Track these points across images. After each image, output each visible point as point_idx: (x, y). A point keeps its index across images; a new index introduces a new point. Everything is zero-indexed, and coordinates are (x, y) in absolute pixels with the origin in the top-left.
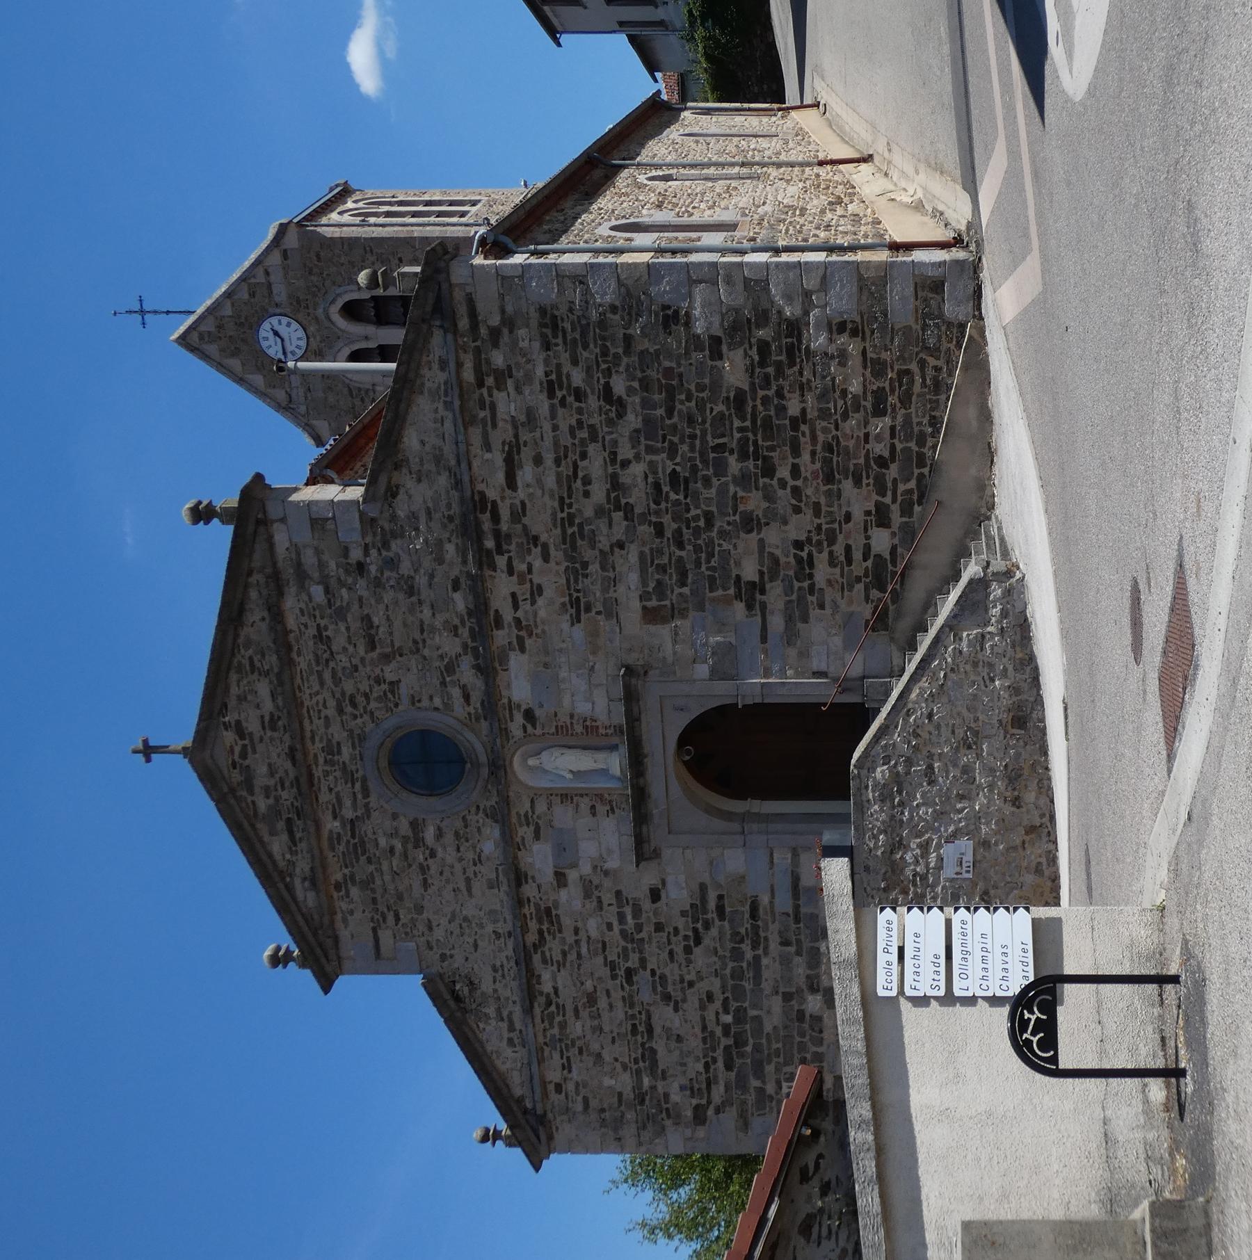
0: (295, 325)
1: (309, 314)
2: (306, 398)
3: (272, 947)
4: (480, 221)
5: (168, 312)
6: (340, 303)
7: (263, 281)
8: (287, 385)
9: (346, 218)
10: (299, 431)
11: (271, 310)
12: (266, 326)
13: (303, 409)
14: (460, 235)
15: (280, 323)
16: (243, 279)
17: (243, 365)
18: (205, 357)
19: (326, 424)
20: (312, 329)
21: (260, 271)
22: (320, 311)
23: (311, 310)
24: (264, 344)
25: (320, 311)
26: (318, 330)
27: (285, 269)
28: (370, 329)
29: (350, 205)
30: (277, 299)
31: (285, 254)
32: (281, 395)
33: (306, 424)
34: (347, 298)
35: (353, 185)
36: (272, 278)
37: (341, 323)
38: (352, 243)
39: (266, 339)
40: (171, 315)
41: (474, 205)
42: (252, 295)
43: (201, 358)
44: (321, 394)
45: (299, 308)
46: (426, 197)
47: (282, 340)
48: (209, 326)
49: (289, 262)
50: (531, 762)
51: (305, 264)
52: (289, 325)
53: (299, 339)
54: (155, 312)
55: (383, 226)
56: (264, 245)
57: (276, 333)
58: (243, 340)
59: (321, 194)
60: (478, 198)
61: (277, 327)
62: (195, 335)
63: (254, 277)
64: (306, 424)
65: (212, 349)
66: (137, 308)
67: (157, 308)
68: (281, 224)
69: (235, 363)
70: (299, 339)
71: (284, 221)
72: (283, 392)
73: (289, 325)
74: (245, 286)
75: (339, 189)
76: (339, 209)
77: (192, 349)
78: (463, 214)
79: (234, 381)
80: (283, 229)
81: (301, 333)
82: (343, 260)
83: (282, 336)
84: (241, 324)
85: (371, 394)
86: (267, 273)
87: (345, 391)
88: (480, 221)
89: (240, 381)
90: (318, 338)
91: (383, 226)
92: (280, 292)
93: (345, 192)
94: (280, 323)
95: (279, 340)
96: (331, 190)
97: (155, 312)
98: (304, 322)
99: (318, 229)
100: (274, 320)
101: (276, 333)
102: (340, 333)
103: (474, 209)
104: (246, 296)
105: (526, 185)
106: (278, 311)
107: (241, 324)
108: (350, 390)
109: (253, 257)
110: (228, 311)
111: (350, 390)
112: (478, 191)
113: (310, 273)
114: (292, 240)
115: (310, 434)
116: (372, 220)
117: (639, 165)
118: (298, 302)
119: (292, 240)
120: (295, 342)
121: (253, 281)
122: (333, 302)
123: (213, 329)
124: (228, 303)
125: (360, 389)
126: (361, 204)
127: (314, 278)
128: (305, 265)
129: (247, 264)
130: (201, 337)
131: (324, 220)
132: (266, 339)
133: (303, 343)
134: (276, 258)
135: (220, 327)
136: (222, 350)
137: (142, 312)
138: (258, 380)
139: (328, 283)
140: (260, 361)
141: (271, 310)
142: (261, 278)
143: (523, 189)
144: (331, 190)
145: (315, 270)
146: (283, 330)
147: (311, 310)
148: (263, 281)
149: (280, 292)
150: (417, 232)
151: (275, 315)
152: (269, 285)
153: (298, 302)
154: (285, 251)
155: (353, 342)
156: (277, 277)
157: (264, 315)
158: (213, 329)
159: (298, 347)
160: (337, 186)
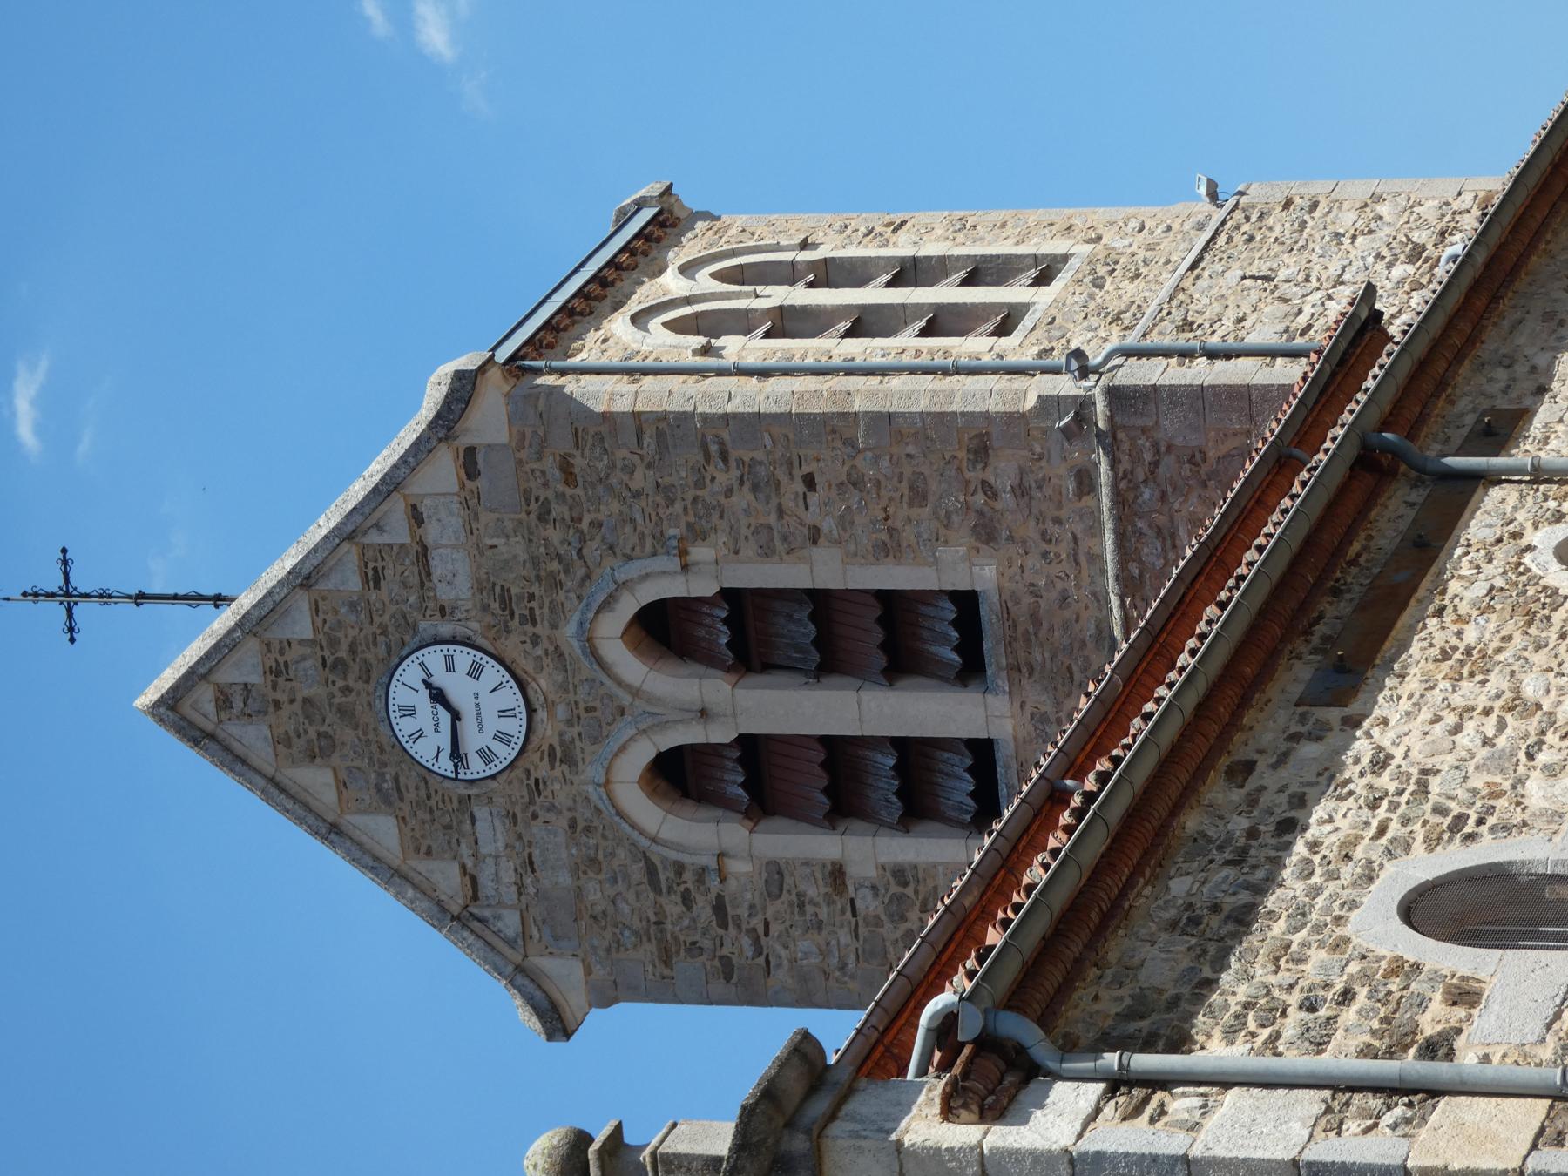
0: (493, 673)
1: (535, 640)
2: (521, 889)
3: (613, 1123)
4: (1059, 358)
5: (141, 598)
6: (628, 607)
7: (406, 539)
8: (465, 850)
9: (660, 342)
10: (498, 987)
11: (426, 626)
12: (410, 673)
13: (510, 923)
14: (994, 406)
15: (450, 666)
16: (347, 533)
17: (342, 785)
18: (234, 761)
19: (577, 968)
20: (543, 683)
21: (396, 510)
22: (569, 630)
23: (542, 629)
24: (404, 727)
25: (569, 630)
26: (563, 687)
27: (471, 504)
28: (715, 688)
29: (671, 283)
30: (445, 594)
31: (470, 463)
32: (447, 878)
33: (519, 969)
34: (650, 593)
35: (689, 197)
36: (431, 532)
37: (630, 666)
38: (661, 432)
39: (408, 711)
40: (147, 607)
41: (1043, 279)
42: (374, 579)
43: (222, 764)
44: (565, 879)
45: (507, 623)
46: (902, 246)
47: (456, 716)
48: (246, 669)
49: (481, 483)
51: (526, 479)
52: (475, 671)
53: (505, 713)
54: (105, 596)
55: (763, 373)
56: (408, 435)
57: (438, 696)
58: (342, 712)
59: (583, 237)
60: (1057, 247)
61: (441, 678)
62: (205, 697)
63: (378, 526)
64: (519, 969)
65: (253, 737)
66: (54, 582)
67: (112, 587)
68: (459, 376)
69: (317, 781)
70: (505, 713)
71: (469, 361)
72: (455, 869)
73: (475, 671)
74: (350, 553)
75: (647, 214)
76: (633, 306)
77: (198, 737)
78: (1007, 322)
79: (315, 833)
80: (464, 387)
81: (511, 697)
82: (637, 482)
83: (460, 706)
84: (339, 666)
85: (713, 883)
86: (416, 517)
87: (637, 871)
88: (1059, 358)
89: (331, 832)
90: (561, 712)
91: (763, 373)
92: (455, 577)
93: (665, 225)
94: (450, 666)
95: (445, 717)
96: (623, 218)
97: (105, 596)
98: (525, 665)
99: (571, 385)
100: (434, 657)
101: (438, 696)
102: (626, 699)
103: (1043, 297)
104: (354, 583)
105: (1213, 195)
106: (446, 629)
107: (339, 666)
108: (651, 871)
109: (377, 468)
110: (301, 626)
111: (651, 871)
112: (1059, 215)
113: (543, 517)
114: (489, 421)
115: (530, 1001)
116: (733, 347)
117: (1539, 476)
118: (505, 600)
119: (489, 421)
120: (493, 724)
121: (374, 538)
122: (608, 604)
123: (255, 678)
124: (303, 602)
125: (680, 868)
126: (704, 281)
127: (555, 535)
128: (527, 495)
129: (358, 490)
130: (223, 701)
131: (588, 351)
132: (408, 711)
133: (516, 727)
134: (443, 472)
135: (277, 672)
136: (282, 741)
137: (68, 595)
138: (383, 830)
139: (593, 550)
140: (393, 778)
141: (426, 626)
142: (398, 532)
143: (1206, 206)
144: (623, 218)
145: (558, 510)
146: (458, 688)
147: (542, 629)
148: (406, 539)
149: (455, 577)
150: (864, 395)
151: (437, 641)
152: (423, 553)
153: (505, 600)
154: (471, 451)
155: (663, 725)
156: (444, 530)
157: (405, 641)
158: (255, 678)
159: (502, 737)
160: (640, 205)
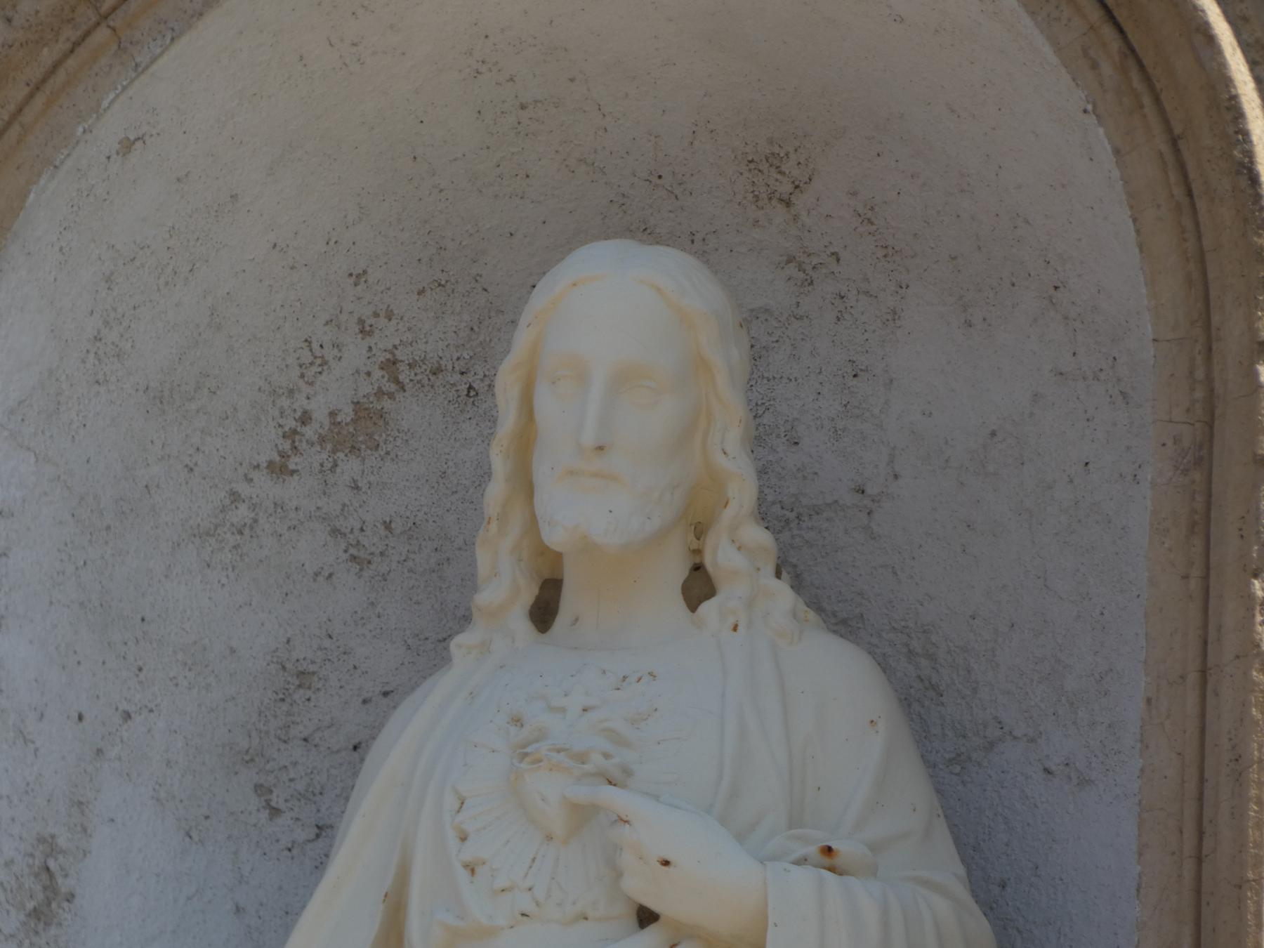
50: (620, 347)
